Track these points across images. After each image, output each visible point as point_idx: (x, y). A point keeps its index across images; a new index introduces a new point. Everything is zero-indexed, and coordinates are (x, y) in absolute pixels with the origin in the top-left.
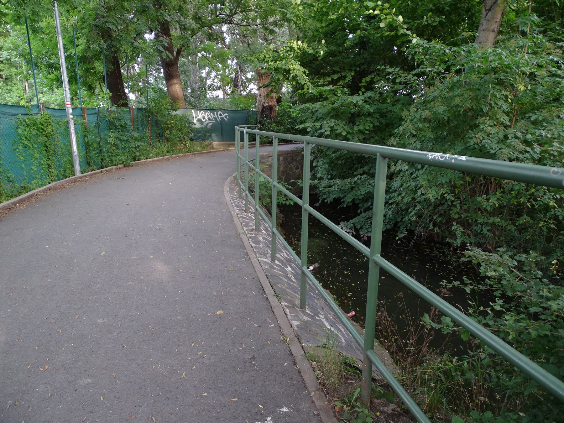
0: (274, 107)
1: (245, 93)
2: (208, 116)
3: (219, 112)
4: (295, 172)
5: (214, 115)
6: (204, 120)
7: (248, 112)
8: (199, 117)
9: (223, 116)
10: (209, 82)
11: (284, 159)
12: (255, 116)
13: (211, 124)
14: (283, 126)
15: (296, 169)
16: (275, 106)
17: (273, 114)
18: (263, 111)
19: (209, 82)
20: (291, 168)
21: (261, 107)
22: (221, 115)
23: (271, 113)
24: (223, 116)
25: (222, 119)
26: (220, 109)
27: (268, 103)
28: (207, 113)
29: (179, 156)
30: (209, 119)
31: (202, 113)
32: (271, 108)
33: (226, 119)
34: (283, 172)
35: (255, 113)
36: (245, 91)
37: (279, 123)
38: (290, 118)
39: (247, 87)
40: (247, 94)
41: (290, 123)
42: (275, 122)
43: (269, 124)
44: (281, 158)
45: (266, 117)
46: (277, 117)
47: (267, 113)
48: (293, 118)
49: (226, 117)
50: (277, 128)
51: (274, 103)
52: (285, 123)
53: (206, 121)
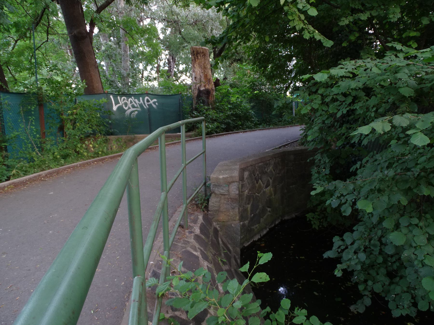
0: (212, 92)
1: (178, 83)
2: (131, 102)
3: (146, 98)
4: (264, 192)
5: (139, 101)
6: (126, 108)
7: (182, 97)
8: (129, 106)
9: (151, 102)
10: (146, 74)
11: (250, 175)
12: (190, 102)
13: (136, 112)
14: (222, 112)
15: (266, 187)
16: (213, 90)
17: (211, 100)
18: (199, 96)
19: (146, 74)
20: (260, 186)
21: (196, 92)
22: (148, 101)
23: (208, 98)
24: (151, 102)
25: (150, 105)
26: (147, 94)
27: (205, 86)
28: (130, 99)
29: (73, 167)
30: (133, 107)
31: (124, 100)
32: (208, 92)
33: (154, 106)
34: (249, 198)
35: (190, 98)
36: (178, 81)
37: (218, 109)
38: (230, 104)
39: (179, 78)
40: (180, 84)
41: (230, 108)
42: (213, 109)
43: (207, 110)
44: (246, 174)
45: (203, 102)
46: (215, 102)
47: (204, 98)
48: (232, 104)
49: (154, 103)
50: (216, 115)
51: (211, 86)
52: (224, 109)
53: (129, 108)
